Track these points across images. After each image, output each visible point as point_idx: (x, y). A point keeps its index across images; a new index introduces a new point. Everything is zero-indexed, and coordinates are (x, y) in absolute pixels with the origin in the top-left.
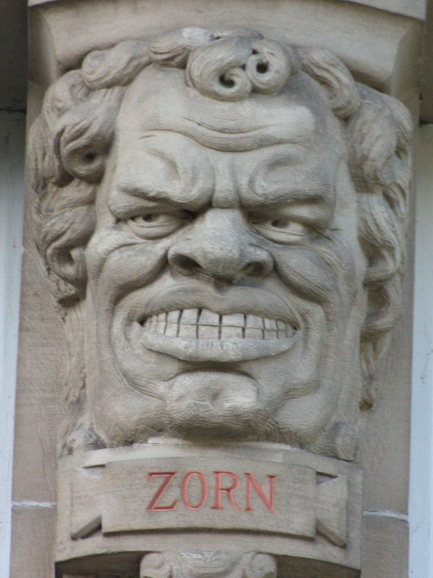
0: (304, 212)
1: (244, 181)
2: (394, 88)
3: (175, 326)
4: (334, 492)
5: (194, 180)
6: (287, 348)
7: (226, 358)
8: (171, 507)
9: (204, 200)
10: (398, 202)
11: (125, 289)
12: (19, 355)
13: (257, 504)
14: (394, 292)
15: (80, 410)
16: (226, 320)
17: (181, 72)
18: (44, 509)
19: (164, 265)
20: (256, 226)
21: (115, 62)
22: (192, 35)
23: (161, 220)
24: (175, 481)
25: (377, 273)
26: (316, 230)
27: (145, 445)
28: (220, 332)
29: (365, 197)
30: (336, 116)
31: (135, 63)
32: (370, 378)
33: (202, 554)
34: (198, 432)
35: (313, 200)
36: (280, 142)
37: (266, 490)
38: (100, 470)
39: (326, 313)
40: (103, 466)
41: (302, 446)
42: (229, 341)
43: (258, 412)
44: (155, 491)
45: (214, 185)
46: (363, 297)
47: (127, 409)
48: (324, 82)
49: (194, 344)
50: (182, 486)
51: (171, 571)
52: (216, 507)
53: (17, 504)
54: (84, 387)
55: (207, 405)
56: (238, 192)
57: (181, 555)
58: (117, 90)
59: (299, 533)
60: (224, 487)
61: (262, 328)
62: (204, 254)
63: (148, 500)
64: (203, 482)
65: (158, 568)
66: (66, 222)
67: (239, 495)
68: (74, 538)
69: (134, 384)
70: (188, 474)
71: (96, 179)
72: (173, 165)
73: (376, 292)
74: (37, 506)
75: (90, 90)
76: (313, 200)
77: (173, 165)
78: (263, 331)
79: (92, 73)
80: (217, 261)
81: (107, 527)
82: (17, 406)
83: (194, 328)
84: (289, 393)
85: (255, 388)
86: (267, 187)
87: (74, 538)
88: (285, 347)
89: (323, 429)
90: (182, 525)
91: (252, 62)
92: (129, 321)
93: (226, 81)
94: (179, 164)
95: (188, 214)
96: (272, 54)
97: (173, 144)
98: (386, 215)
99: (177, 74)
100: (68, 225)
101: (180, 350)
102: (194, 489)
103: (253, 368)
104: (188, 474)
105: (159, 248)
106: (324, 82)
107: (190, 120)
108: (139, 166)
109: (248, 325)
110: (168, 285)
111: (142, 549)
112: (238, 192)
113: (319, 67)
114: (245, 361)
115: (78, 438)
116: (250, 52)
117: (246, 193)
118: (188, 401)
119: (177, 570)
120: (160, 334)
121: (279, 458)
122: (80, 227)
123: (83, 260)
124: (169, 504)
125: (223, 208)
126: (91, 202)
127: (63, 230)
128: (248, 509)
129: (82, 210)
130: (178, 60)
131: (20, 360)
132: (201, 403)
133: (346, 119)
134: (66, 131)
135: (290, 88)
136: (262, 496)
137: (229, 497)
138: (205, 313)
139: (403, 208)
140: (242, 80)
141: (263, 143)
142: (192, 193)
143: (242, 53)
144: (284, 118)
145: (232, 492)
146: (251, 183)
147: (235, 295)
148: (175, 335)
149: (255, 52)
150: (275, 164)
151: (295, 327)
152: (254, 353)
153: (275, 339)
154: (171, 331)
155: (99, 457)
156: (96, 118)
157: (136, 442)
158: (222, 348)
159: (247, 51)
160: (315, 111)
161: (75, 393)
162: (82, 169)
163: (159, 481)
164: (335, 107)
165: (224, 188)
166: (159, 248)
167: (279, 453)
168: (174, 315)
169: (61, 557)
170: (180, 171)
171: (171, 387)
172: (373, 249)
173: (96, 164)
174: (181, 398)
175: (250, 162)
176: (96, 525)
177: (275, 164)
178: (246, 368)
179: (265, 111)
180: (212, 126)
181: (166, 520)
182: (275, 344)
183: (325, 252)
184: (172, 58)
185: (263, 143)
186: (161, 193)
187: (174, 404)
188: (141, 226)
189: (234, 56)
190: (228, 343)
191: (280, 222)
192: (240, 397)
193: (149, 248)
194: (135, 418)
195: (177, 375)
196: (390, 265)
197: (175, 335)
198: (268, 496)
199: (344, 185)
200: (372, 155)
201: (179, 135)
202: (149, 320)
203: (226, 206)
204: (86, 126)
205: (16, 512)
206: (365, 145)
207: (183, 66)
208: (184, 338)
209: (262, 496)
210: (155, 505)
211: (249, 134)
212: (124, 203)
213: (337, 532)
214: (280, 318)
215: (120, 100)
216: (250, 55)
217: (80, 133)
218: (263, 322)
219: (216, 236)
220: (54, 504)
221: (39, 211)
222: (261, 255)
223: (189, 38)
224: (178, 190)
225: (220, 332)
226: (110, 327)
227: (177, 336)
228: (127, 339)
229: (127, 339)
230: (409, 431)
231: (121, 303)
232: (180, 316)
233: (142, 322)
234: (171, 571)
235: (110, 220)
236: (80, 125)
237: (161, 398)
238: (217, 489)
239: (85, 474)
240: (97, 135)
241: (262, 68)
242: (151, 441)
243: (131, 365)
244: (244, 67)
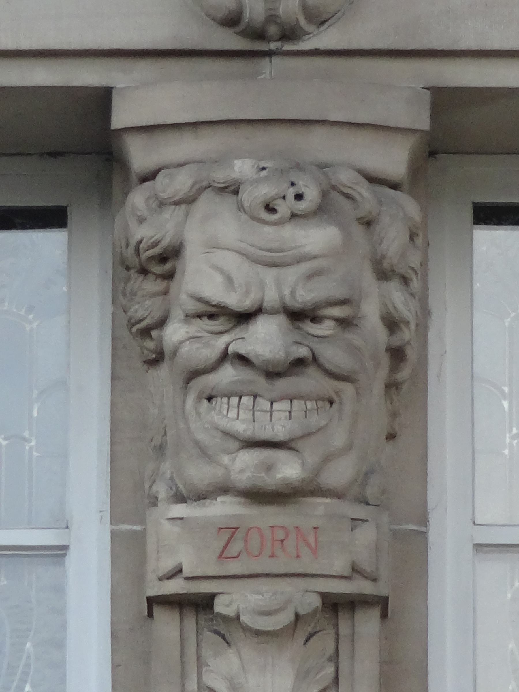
0: (336, 312)
1: (287, 292)
2: (370, 520)
3: (236, 410)
4: (366, 535)
5: (247, 293)
6: (325, 423)
7: (276, 439)
8: (238, 556)
9: (256, 306)
10: (412, 280)
11: (194, 374)
12: (112, 400)
13: (305, 551)
14: (411, 354)
15: (162, 455)
16: (276, 406)
17: (234, 197)
18: (135, 532)
19: (225, 357)
20: (297, 323)
21: (180, 183)
22: (242, 168)
23: (222, 319)
24: (239, 535)
25: (396, 341)
26: (344, 323)
27: (214, 502)
28: (271, 416)
29: (385, 285)
30: (360, 223)
31: (197, 186)
32: (394, 415)
33: (263, 596)
34: (258, 496)
35: (343, 302)
36: (315, 257)
37: (311, 539)
38: (180, 522)
39: (357, 389)
40: (182, 519)
41: (339, 498)
42: (279, 424)
43: (303, 480)
44: (223, 544)
45: (263, 296)
46: (385, 360)
47: (200, 474)
48: (348, 196)
49: (251, 427)
50: (246, 540)
51: (238, 608)
52: (272, 556)
53: (113, 527)
54: (165, 434)
55: (263, 477)
56: (282, 299)
57: (246, 596)
58: (183, 207)
59: (339, 574)
60: (279, 539)
61: (305, 410)
62: (257, 356)
63: (219, 551)
64: (262, 536)
65: (228, 606)
66: (146, 310)
67: (290, 543)
68: (160, 579)
69: (204, 453)
70: (249, 529)
71: (169, 276)
72: (229, 280)
73: (397, 354)
74: (131, 529)
75: (162, 204)
76: (343, 302)
77: (229, 280)
78: (306, 412)
79: (164, 192)
80: (268, 362)
81: (187, 571)
82: (112, 443)
83: (252, 412)
84: (327, 459)
85: (300, 461)
86: (305, 296)
87: (160, 579)
88: (323, 423)
89: (356, 480)
90: (246, 573)
91: (291, 192)
92: (199, 398)
93: (270, 209)
94: (235, 280)
95: (244, 317)
96: (306, 186)
97: (231, 262)
98: (403, 298)
99: (231, 199)
100: (148, 313)
101: (240, 432)
102: (255, 542)
103: (299, 445)
104: (249, 529)
105: (221, 342)
106: (348, 196)
107: (243, 242)
108: (204, 277)
109: (294, 409)
110: (228, 374)
111: (215, 591)
112: (282, 299)
113: (345, 186)
114: (293, 440)
115: (161, 490)
116: (290, 183)
117: (289, 302)
118: (248, 474)
119: (243, 608)
120: (224, 415)
121: (320, 511)
122: (157, 315)
123: (160, 340)
124: (236, 554)
125: (271, 314)
126: (166, 292)
127: (145, 316)
128: (298, 556)
129: (159, 300)
130: (232, 188)
131: (113, 405)
132: (258, 475)
133: (368, 223)
134: (145, 240)
135: (322, 211)
136: (309, 546)
137: (282, 546)
138: (258, 399)
139: (416, 284)
140: (283, 209)
141: (300, 260)
142: (245, 304)
143: (284, 187)
144: (317, 238)
145: (285, 542)
146: (293, 293)
147: (283, 385)
148: (237, 416)
149: (293, 184)
150: (311, 276)
151: (331, 403)
152: (299, 433)
153: (316, 416)
154: (233, 414)
155: (179, 510)
156: (168, 232)
157: (208, 499)
158: (273, 430)
159: (287, 184)
160: (343, 227)
161: (157, 441)
162: (158, 269)
163: (226, 536)
164: (359, 217)
165: (271, 297)
166: (221, 342)
167: (321, 505)
168: (235, 400)
169: (152, 593)
170: (236, 286)
171: (234, 460)
172: (392, 324)
173: (168, 266)
174: (242, 471)
175: (291, 275)
176: (177, 570)
177: (311, 276)
178: (293, 445)
179: (302, 232)
180: (260, 247)
181: (234, 567)
182: (315, 420)
183: (354, 339)
184: (226, 187)
185: (300, 260)
186: (220, 302)
187: (237, 475)
188: (207, 324)
189: (276, 190)
190: (279, 427)
191: (315, 319)
192: (289, 469)
193: (213, 342)
194: (206, 482)
195: (239, 449)
196: (407, 334)
197: (237, 416)
198: (313, 545)
199: (368, 278)
200: (389, 254)
201: (234, 253)
202: (214, 399)
203: (273, 312)
204: (160, 239)
205: (113, 534)
206: (384, 246)
207: (236, 192)
208: (244, 421)
209: (309, 546)
210: (223, 556)
211: (290, 253)
212: (192, 306)
213: (369, 570)
214: (318, 399)
215: (187, 215)
216: (289, 188)
217: (155, 245)
218: (305, 404)
219: (265, 339)
220: (144, 527)
221: (124, 295)
222: (303, 352)
223: (240, 172)
224: (234, 301)
225: (271, 416)
226: (184, 401)
227: (238, 419)
228: (198, 414)
229: (198, 414)
230: (426, 456)
231: (191, 384)
232: (240, 401)
233: (210, 399)
234: (238, 608)
235: (182, 316)
236: (156, 237)
237: (226, 467)
238: (274, 541)
239: (167, 526)
240: (169, 245)
241: (299, 197)
242: (219, 499)
243: (201, 436)
244: (284, 197)
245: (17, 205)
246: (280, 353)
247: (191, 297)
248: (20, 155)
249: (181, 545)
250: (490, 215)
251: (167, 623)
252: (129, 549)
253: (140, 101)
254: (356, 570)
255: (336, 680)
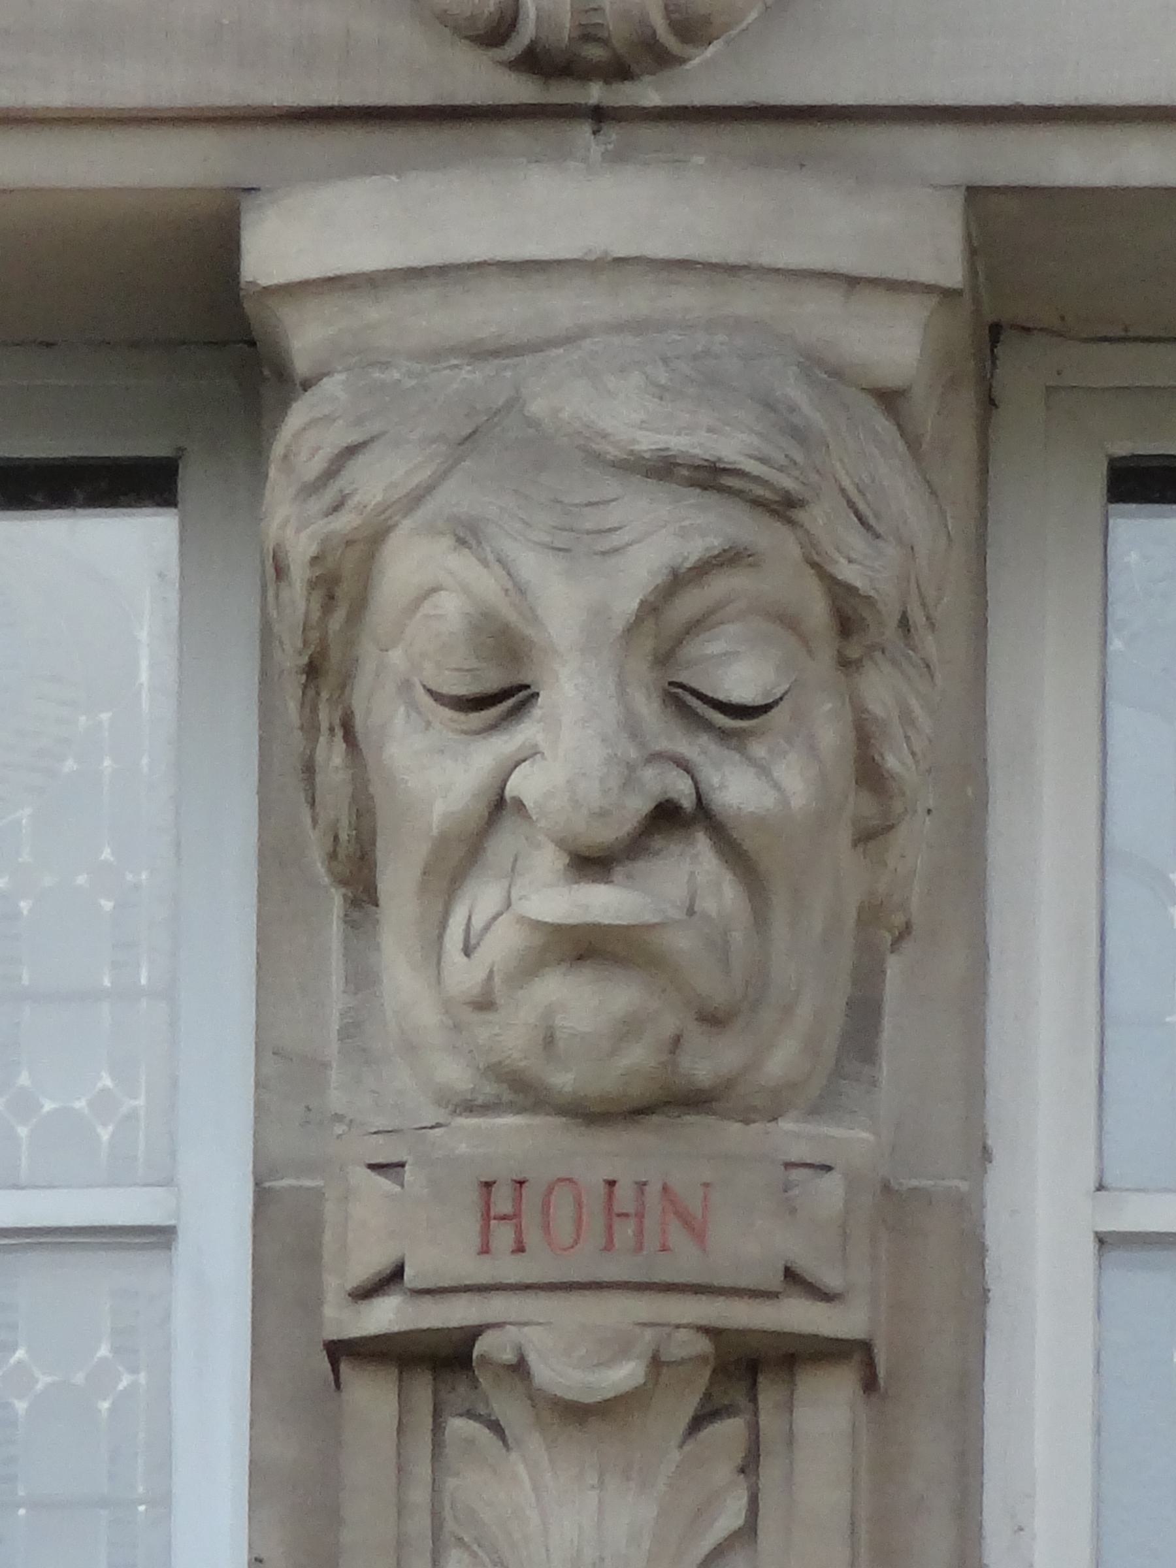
13: (678, 1237)
108: (430, 592)
169: (333, 1333)
245: (55, 455)
246: (708, 905)
247: (690, 1434)
248: (108, 366)
249: (403, 1235)
250: (1143, 482)
251: (372, 1397)
252: (286, 1229)
253: (306, 235)
254: (794, 1279)
255: (749, 1530)
